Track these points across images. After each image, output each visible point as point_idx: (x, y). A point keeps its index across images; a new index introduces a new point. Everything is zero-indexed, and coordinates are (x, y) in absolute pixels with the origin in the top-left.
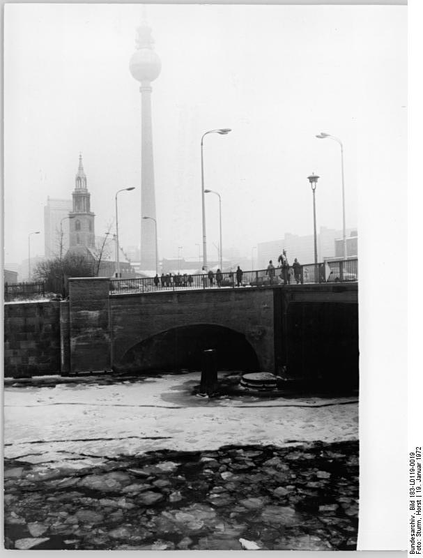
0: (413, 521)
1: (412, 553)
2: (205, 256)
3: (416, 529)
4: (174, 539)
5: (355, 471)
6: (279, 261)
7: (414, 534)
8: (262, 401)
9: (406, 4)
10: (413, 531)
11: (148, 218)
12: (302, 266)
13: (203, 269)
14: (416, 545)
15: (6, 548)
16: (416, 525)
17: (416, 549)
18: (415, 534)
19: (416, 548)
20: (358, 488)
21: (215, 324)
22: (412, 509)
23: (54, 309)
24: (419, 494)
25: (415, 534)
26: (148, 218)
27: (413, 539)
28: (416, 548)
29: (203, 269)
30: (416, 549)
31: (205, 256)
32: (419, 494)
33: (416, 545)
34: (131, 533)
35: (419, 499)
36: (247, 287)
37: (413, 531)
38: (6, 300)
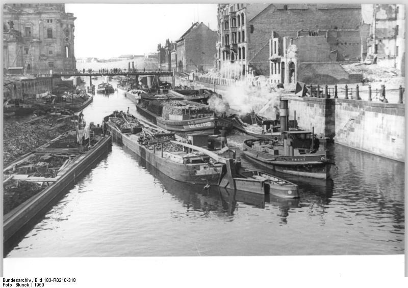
0: (27, 281)
1: (4, 280)
2: (362, 91)
3: (20, 283)
4: (6, 44)
7: (18, 282)
9: (406, 275)
10: (20, 281)
13: (50, 53)
14: (10, 283)
16: (24, 283)
18: (18, 282)
19: (7, 283)
21: (254, 133)
22: (36, 280)
23: (83, 137)
25: (18, 282)
27: (14, 280)
28: (7, 283)
29: (50, 53)
31: (362, 91)
33: (10, 283)
35: (30, 285)
36: (276, 180)
37: (20, 281)
38: (92, 125)
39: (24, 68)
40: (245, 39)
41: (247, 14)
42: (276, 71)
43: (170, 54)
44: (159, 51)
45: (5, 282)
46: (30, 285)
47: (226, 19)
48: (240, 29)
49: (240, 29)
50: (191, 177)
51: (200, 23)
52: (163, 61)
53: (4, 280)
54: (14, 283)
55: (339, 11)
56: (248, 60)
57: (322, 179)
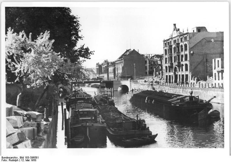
1: (2, 157)
5: (48, 148)
6: (17, 148)
8: (21, 110)
10: (11, 158)
11: (131, 84)
12: (210, 101)
14: (5, 159)
15: (69, 147)
16: (14, 159)
17: (4, 159)
19: (4, 159)
20: (49, 148)
22: (20, 157)
24: (21, 160)
26: (131, 84)
27: (8, 158)
28: (4, 159)
30: (4, 159)
32: (21, 160)
33: (5, 159)
34: (77, 70)
35: (19, 160)
37: (11, 158)
39: (154, 99)
40: (188, 59)
41: (189, 44)
42: (219, 77)
43: (108, 68)
44: (98, 67)
45: (3, 159)
46: (19, 160)
47: (170, 48)
48: (183, 53)
49: (183, 53)
50: (214, 137)
51: (132, 50)
52: (100, 73)
53: (2, 157)
54: (8, 159)
55: (219, 40)
56: (191, 71)
57: (64, 103)
